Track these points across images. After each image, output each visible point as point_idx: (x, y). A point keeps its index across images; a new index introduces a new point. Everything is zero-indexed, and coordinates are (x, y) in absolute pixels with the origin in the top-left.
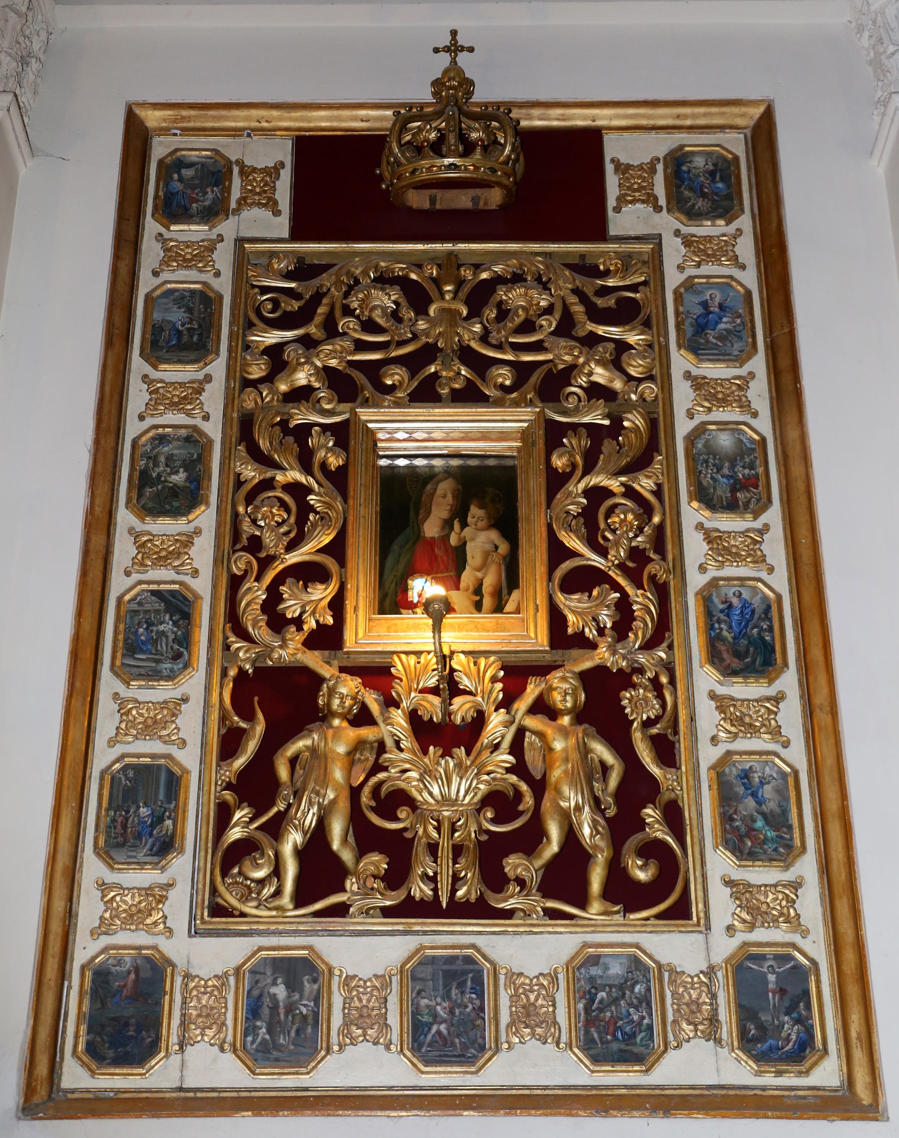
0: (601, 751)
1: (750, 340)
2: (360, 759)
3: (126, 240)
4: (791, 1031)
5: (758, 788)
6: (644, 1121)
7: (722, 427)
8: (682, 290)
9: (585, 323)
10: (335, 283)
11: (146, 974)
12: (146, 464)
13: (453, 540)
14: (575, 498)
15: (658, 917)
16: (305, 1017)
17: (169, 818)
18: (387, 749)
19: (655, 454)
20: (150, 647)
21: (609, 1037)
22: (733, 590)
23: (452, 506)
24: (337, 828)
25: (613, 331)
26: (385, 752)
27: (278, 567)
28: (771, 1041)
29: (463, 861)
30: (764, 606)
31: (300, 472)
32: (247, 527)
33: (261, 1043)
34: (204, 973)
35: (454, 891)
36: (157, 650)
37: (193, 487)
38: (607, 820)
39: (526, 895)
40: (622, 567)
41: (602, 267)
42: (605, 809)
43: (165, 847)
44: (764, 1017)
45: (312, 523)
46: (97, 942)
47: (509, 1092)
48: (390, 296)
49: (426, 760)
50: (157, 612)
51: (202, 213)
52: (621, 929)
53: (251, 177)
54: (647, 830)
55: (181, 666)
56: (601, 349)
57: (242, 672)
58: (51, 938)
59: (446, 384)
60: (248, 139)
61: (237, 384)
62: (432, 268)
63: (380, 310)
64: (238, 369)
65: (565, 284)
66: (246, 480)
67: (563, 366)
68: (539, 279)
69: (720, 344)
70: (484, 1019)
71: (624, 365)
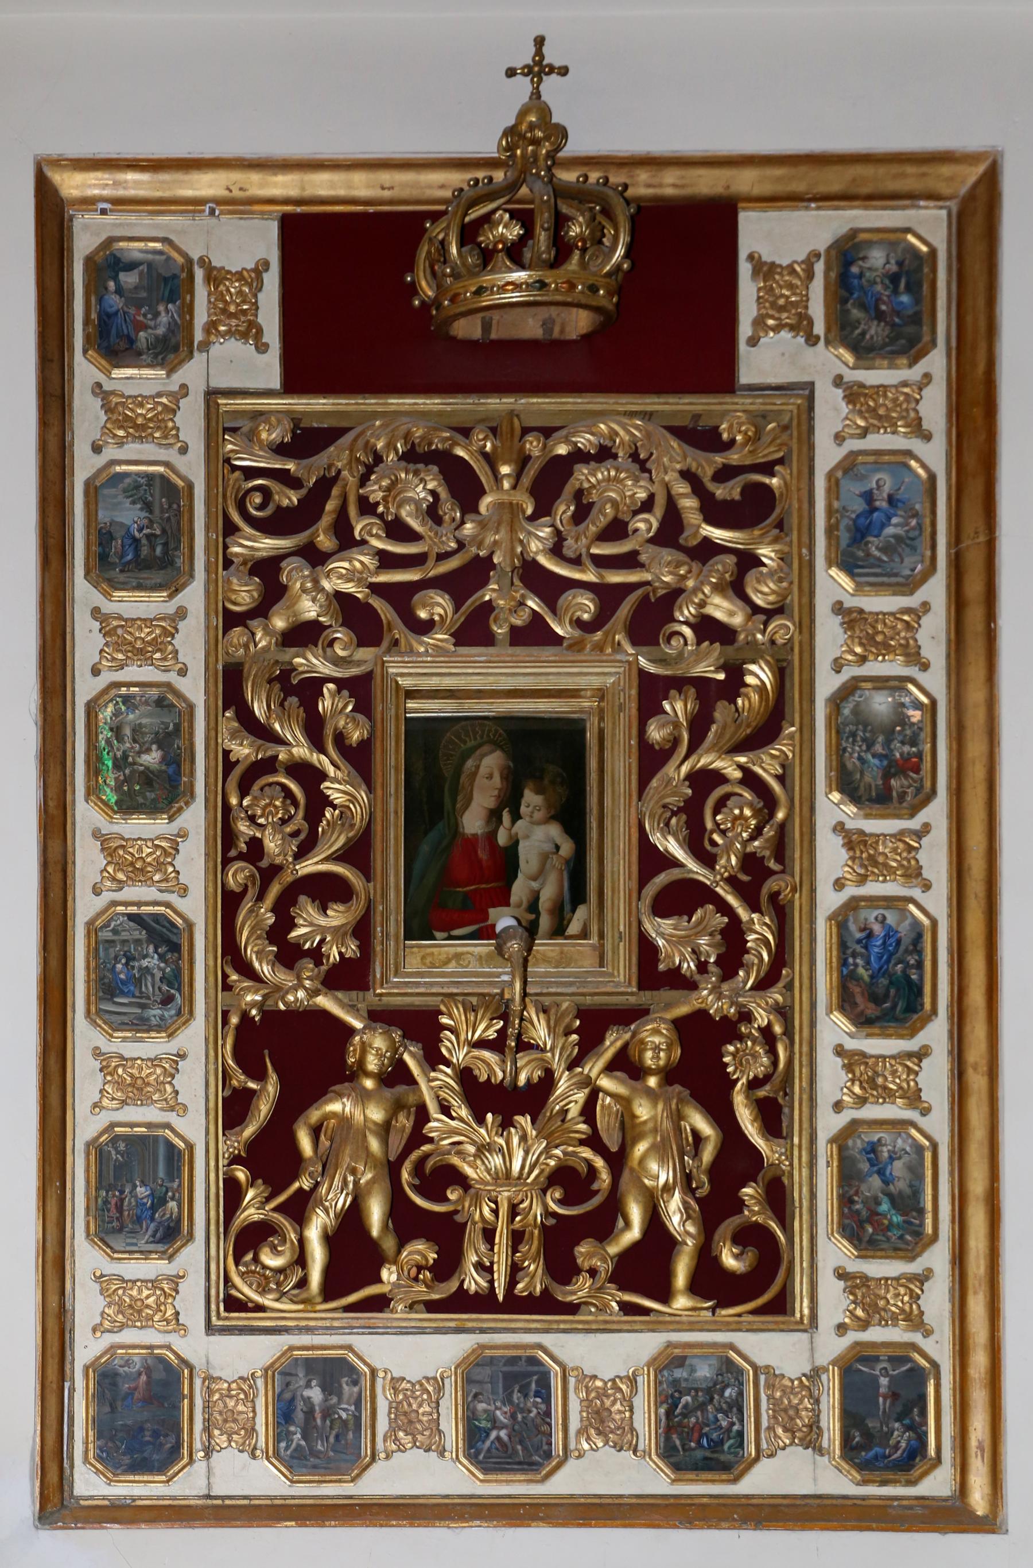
13: (502, 838)
15: (754, 1312)
16: (345, 1422)
17: (173, 1199)
21: (693, 1444)
23: (500, 790)
24: (376, 1213)
27: (288, 878)
30: (913, 935)
32: (243, 827)
33: (295, 1450)
36: (141, 992)
38: (698, 1201)
40: (732, 881)
41: (725, 436)
42: (697, 1188)
50: (138, 942)
54: (746, 1213)
55: (173, 1012)
56: (720, 567)
65: (672, 458)
66: (238, 761)
68: (634, 456)
69: (885, 558)
70: (550, 1425)
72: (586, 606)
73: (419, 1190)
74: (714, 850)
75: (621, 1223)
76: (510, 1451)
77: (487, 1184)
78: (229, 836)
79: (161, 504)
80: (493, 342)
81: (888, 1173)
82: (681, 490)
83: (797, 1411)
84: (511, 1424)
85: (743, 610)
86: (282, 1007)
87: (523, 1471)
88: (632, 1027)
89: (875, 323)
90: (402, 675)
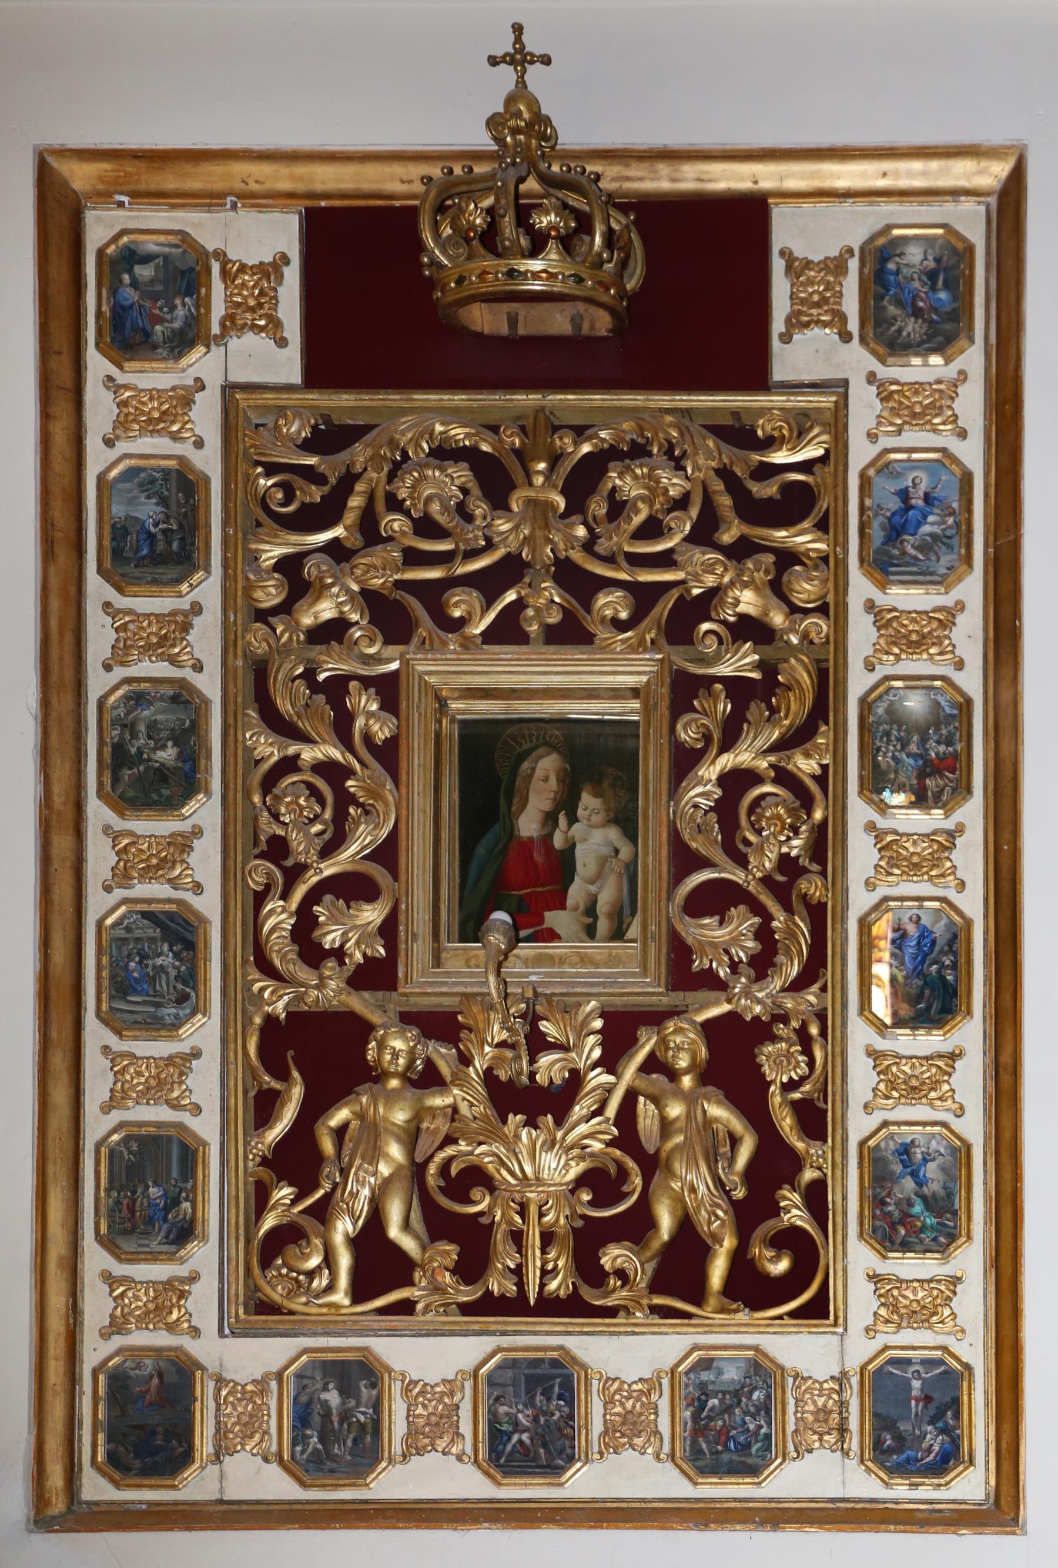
1: (963, 551)
3: (59, 388)
4: (934, 1441)
5: (920, 1166)
6: (746, 1535)
7: (911, 683)
8: (871, 472)
11: (171, 1378)
12: (121, 736)
16: (362, 1426)
17: (186, 1199)
19: (820, 722)
20: (146, 986)
21: (720, 1448)
22: (910, 913)
23: (556, 793)
28: (909, 1452)
30: (949, 936)
33: (312, 1453)
34: (241, 1377)
36: (155, 991)
37: (187, 768)
38: (735, 1204)
41: (760, 433)
43: (185, 1233)
44: (903, 1427)
46: (110, 1343)
47: (603, 1505)
50: (152, 940)
51: (171, 341)
52: (742, 1329)
53: (238, 281)
55: (188, 1011)
56: (751, 566)
58: (51, 1338)
60: (232, 214)
65: (706, 458)
68: (669, 451)
69: (921, 557)
70: (573, 1428)
71: (785, 589)
76: (532, 1454)
79: (178, 499)
80: (525, 339)
81: (921, 1174)
82: (717, 488)
83: (818, 1411)
84: (532, 1428)
87: (544, 1475)
89: (913, 319)
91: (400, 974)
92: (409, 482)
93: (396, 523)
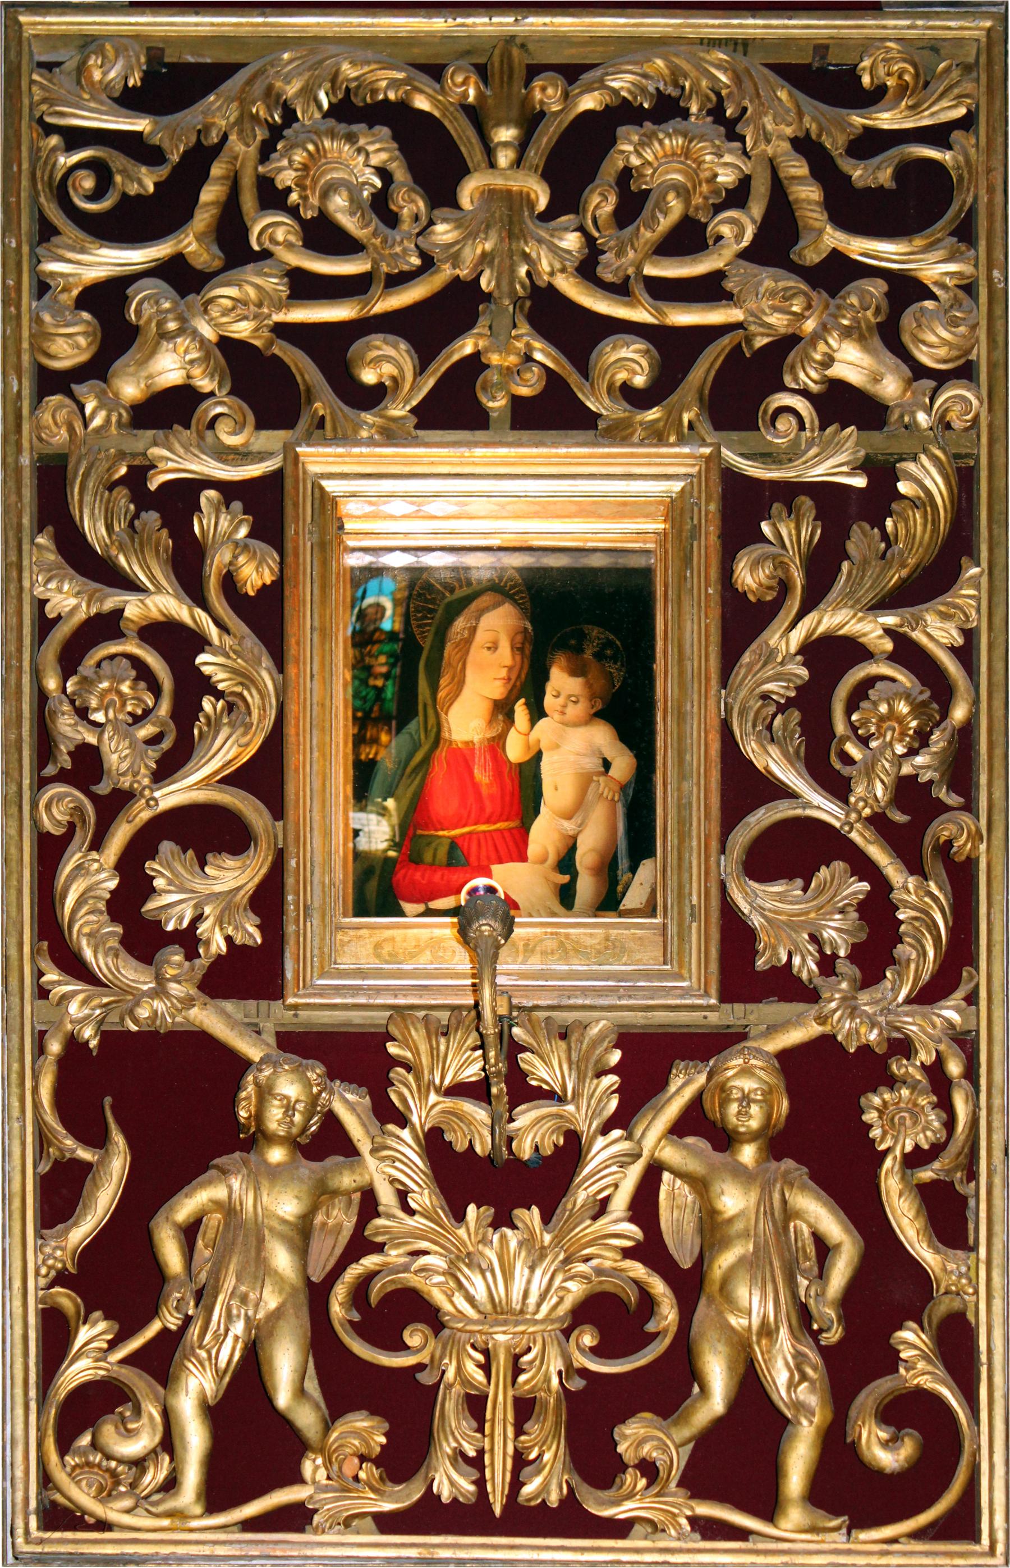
0: (818, 1214)
2: (324, 1224)
9: (821, 232)
10: (239, 121)
13: (515, 751)
14: (782, 663)
15: (917, 1535)
18: (381, 1209)
19: (964, 560)
23: (510, 669)
24: (286, 1366)
25: (886, 251)
26: (378, 1215)
27: (141, 814)
29: (534, 1428)
31: (177, 596)
32: (69, 729)
35: (516, 1485)
38: (825, 1352)
39: (658, 1495)
40: (878, 822)
41: (866, 80)
42: (821, 1331)
45: (208, 718)
48: (367, 154)
49: (462, 1232)
54: (902, 1371)
56: (854, 300)
57: (74, 1045)
59: (502, 386)
61: (26, 383)
62: (465, 83)
63: (345, 194)
64: (25, 345)
65: (779, 120)
66: (59, 617)
67: (766, 340)
68: (717, 112)
71: (906, 339)
72: (629, 362)
73: (360, 1329)
74: (846, 771)
75: (696, 1389)
77: (470, 1321)
78: (45, 744)
82: (793, 171)
85: (896, 370)
86: (134, 1028)
88: (711, 1063)
90: (331, 476)
91: (289, 975)
92: (299, 157)
93: (272, 230)
